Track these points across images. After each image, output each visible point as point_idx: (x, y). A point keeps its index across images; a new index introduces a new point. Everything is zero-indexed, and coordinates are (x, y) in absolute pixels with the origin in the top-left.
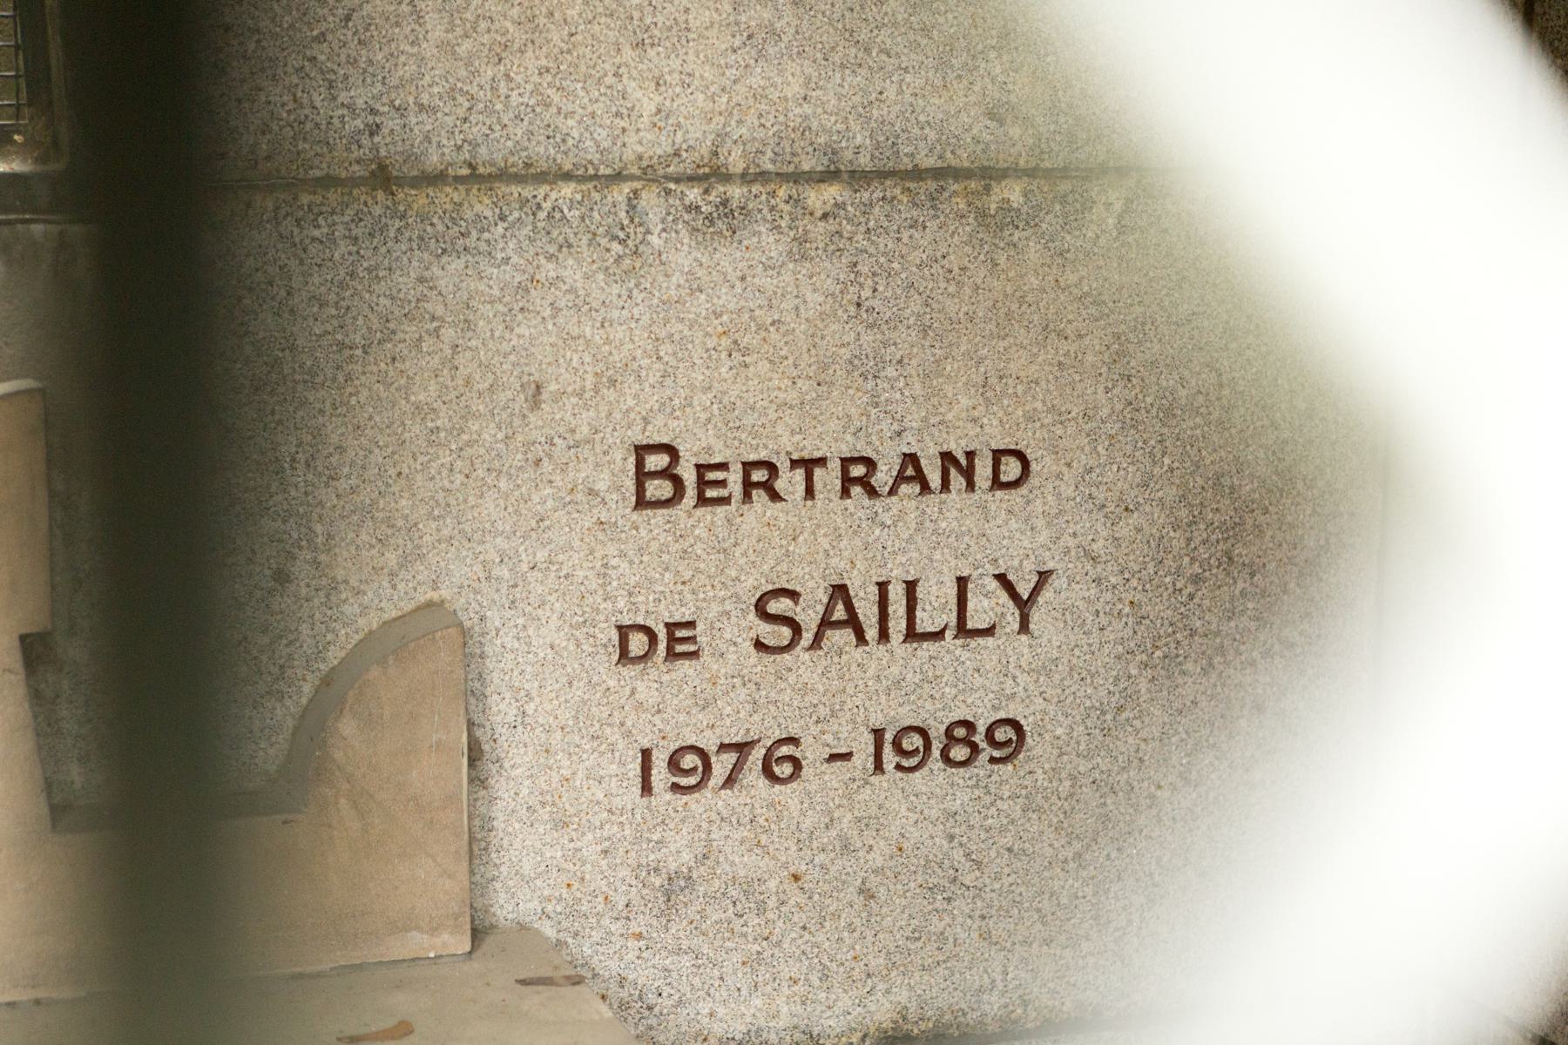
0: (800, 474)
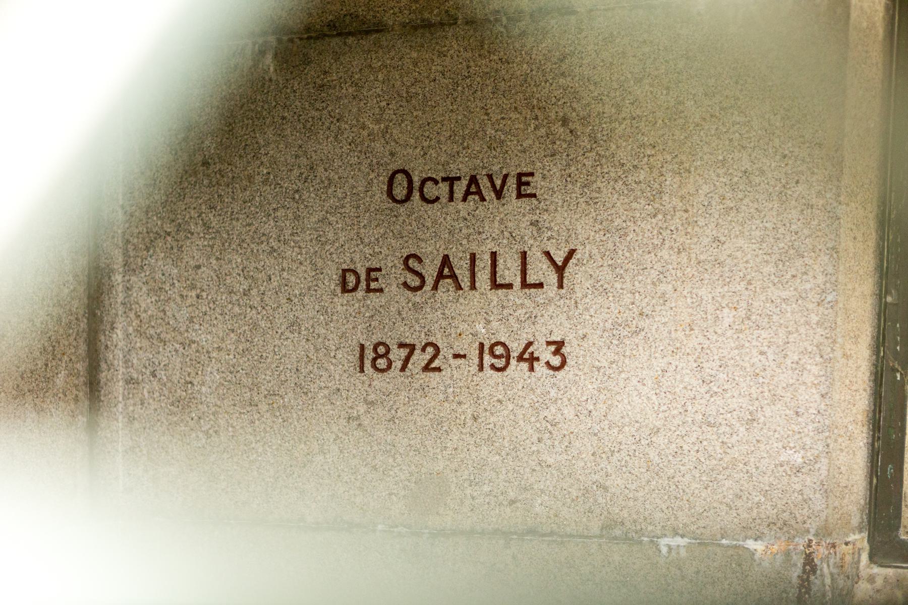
0: (447, 184)
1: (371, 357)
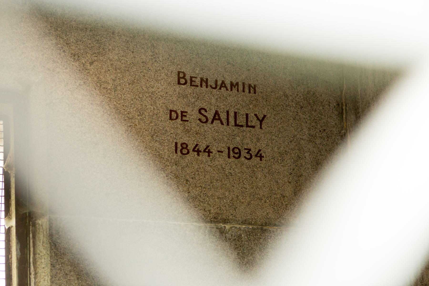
1: (180, 149)
